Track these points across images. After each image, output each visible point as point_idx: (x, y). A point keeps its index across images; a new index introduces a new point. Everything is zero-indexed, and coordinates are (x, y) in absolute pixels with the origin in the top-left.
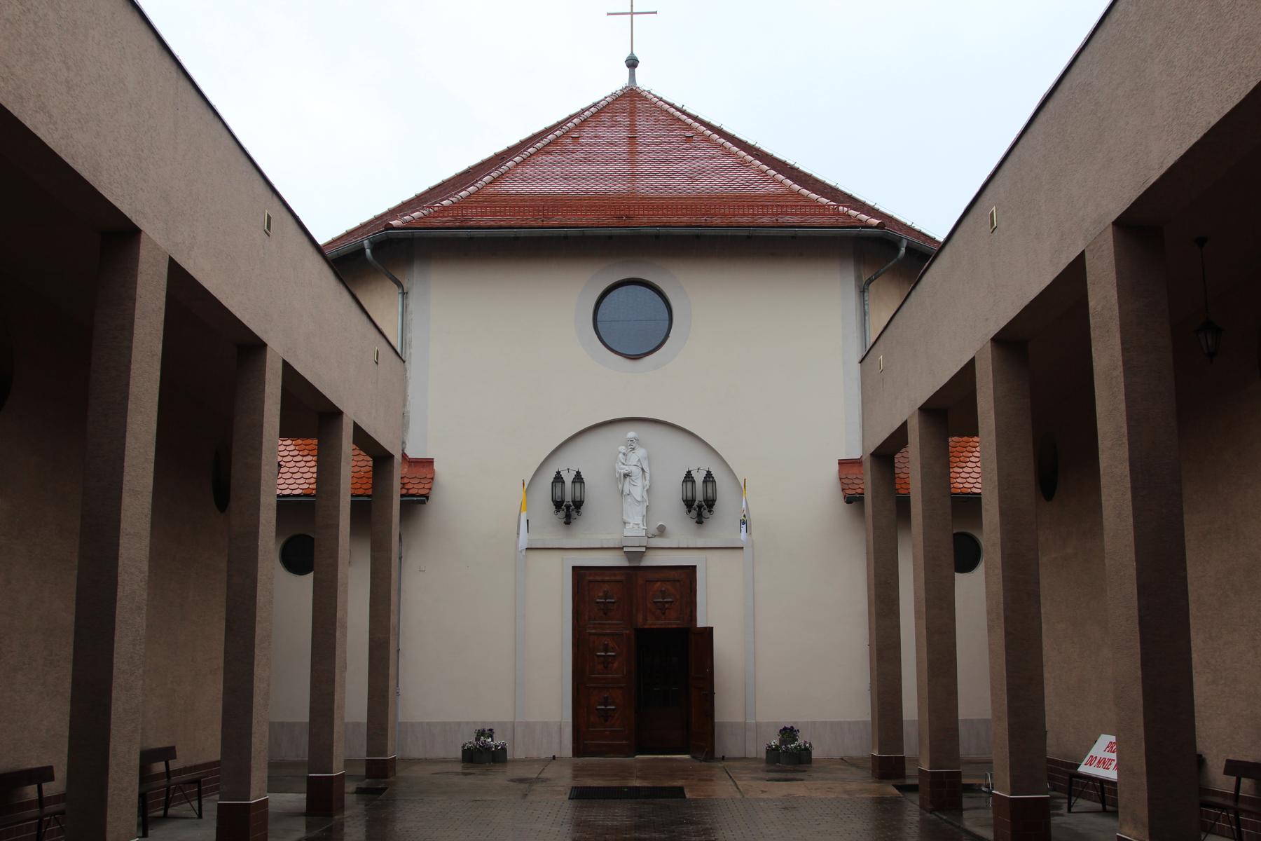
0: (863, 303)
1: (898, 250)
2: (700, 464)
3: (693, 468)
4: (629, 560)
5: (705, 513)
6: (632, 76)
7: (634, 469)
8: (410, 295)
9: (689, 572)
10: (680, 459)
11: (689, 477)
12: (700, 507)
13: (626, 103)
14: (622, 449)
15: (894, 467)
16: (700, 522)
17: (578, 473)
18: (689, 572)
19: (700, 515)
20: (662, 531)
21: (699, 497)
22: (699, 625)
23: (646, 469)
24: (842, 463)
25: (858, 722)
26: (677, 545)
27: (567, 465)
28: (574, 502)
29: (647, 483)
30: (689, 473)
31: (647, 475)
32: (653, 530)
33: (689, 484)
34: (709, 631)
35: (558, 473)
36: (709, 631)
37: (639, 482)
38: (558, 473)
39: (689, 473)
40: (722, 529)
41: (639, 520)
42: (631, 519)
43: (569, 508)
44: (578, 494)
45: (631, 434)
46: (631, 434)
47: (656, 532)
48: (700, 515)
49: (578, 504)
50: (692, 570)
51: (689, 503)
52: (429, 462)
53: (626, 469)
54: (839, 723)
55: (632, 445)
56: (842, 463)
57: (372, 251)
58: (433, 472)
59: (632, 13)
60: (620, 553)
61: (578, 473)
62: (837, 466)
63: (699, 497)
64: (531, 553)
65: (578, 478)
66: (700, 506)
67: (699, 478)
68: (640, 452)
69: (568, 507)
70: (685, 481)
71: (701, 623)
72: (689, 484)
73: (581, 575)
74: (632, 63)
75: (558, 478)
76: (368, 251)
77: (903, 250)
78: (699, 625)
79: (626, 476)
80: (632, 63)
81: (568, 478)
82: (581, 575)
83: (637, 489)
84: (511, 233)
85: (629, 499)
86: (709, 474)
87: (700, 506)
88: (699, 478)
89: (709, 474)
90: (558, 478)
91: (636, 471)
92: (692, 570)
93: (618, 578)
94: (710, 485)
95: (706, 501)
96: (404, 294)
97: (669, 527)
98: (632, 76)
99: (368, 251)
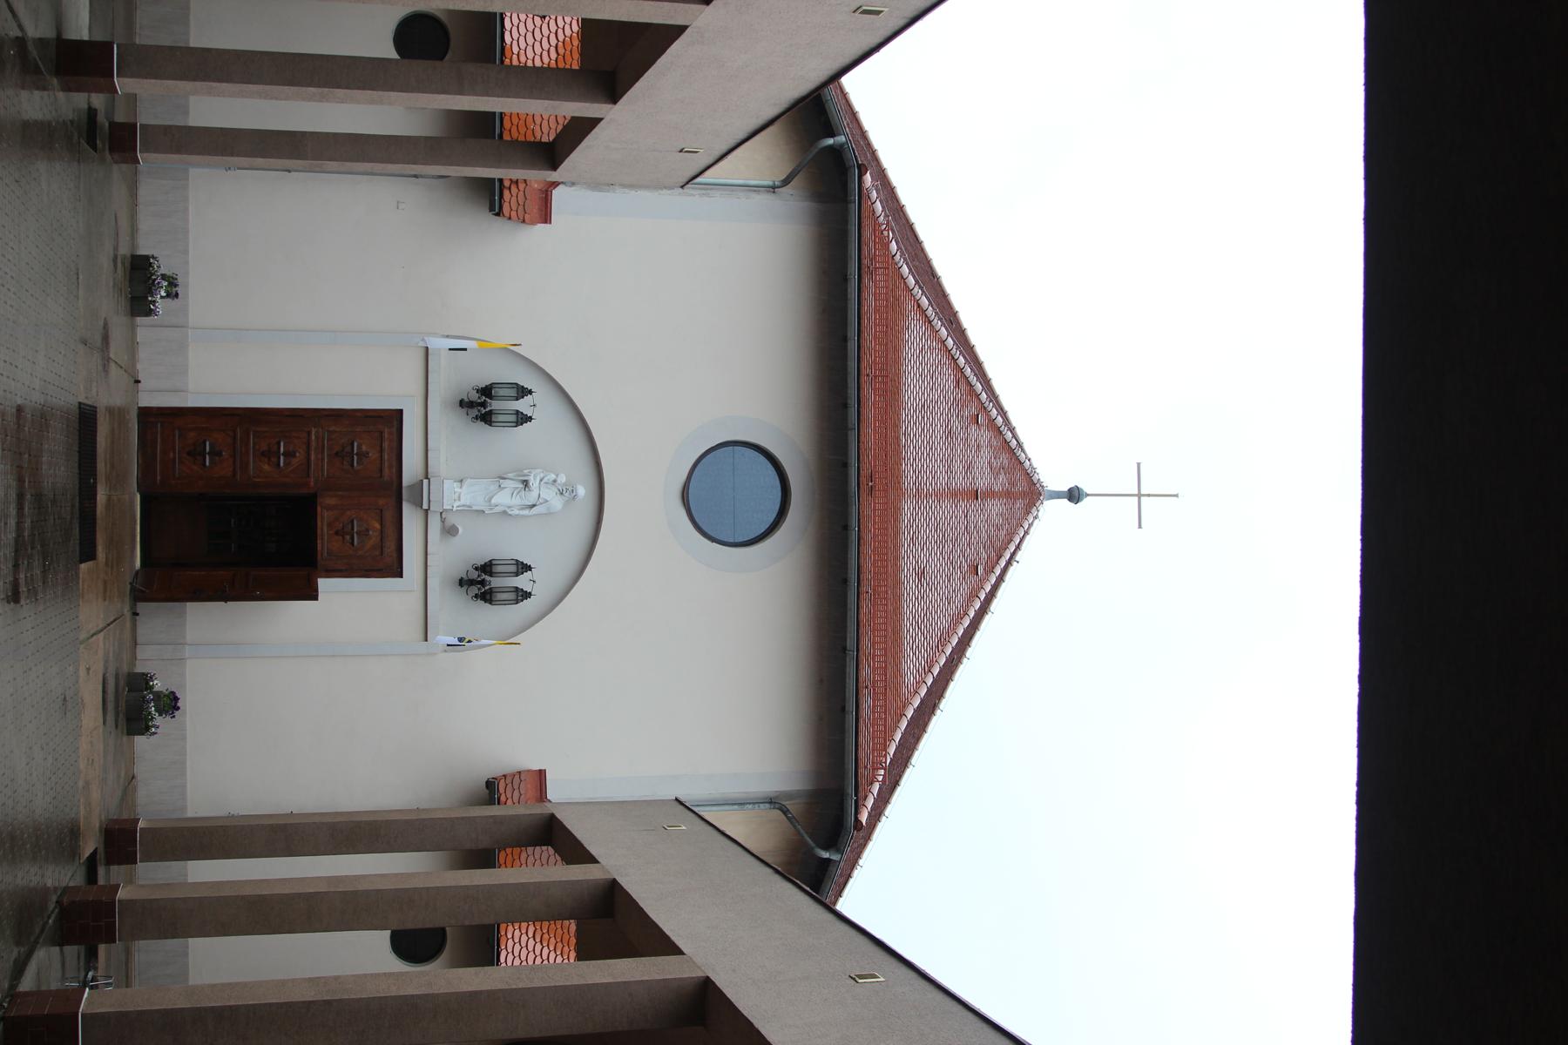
1: (826, 848)
2: (540, 583)
4: (411, 487)
6: (1057, 495)
7: (534, 494)
10: (545, 550)
11: (524, 568)
14: (562, 479)
16: (461, 582)
17: (530, 419)
19: (471, 582)
24: (541, 774)
27: (540, 404)
29: (516, 512)
30: (529, 568)
31: (526, 512)
32: (452, 520)
33: (513, 569)
34: (313, 595)
36: (313, 595)
37: (517, 501)
38: (530, 392)
39: (529, 568)
40: (455, 613)
42: (464, 488)
43: (482, 405)
44: (501, 418)
45: (581, 491)
46: (581, 491)
48: (471, 582)
49: (487, 418)
51: (487, 568)
52: (546, 217)
53: (534, 483)
55: (566, 492)
56: (541, 774)
57: (831, 147)
58: (533, 223)
59: (1139, 495)
64: (422, 353)
65: (522, 419)
66: (482, 583)
67: (522, 582)
68: (557, 503)
69: (483, 405)
71: (323, 584)
72: (513, 569)
73: (394, 419)
74: (1074, 495)
75: (523, 392)
76: (830, 141)
77: (825, 855)
79: (526, 483)
80: (1074, 495)
81: (523, 405)
82: (394, 419)
83: (506, 498)
85: (493, 487)
86: (527, 595)
87: (482, 583)
88: (522, 582)
89: (527, 595)
90: (523, 392)
91: (532, 497)
93: (386, 471)
96: (773, 189)
97: (456, 540)
98: (1057, 495)
99: (830, 141)
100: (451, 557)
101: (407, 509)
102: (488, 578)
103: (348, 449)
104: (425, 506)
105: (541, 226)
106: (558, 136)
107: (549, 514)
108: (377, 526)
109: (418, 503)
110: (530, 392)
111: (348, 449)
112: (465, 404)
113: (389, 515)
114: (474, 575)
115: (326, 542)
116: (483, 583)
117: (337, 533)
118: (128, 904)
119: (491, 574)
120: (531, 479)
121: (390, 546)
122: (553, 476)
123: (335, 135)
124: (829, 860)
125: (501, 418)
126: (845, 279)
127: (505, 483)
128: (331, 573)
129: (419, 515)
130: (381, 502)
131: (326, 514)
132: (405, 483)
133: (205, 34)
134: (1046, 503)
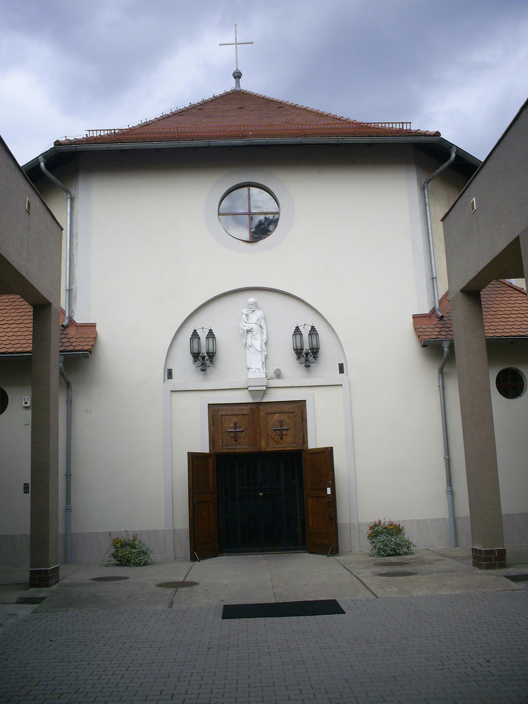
1: (450, 155)
2: (305, 320)
4: (253, 397)
5: (311, 358)
6: (238, 84)
7: (255, 327)
8: (76, 200)
9: (301, 404)
10: (287, 319)
12: (307, 354)
13: (194, 336)
14: (245, 311)
15: (481, 305)
16: (308, 366)
17: (211, 331)
18: (301, 404)
19: (307, 360)
20: (278, 375)
21: (307, 347)
22: (310, 447)
24: (415, 317)
25: (437, 520)
27: (202, 324)
29: (265, 337)
30: (297, 328)
31: (265, 331)
32: (271, 374)
33: (298, 337)
34: (327, 454)
35: (195, 331)
36: (327, 454)
37: (258, 336)
38: (195, 331)
39: (297, 328)
40: (326, 370)
41: (259, 365)
42: (253, 364)
43: (204, 359)
44: (211, 347)
45: (251, 300)
46: (251, 300)
47: (273, 375)
48: (307, 360)
49: (212, 355)
50: (302, 403)
51: (299, 352)
52: (93, 326)
53: (248, 327)
54: (425, 521)
55: (254, 308)
56: (415, 317)
57: (46, 165)
58: (96, 333)
59: (236, 44)
60: (246, 392)
61: (211, 331)
62: (411, 320)
63: (307, 347)
64: (175, 395)
65: (211, 335)
66: (308, 355)
67: (305, 332)
68: (259, 313)
69: (203, 358)
71: (315, 441)
72: (298, 337)
73: (214, 409)
74: (237, 76)
75: (195, 335)
76: (42, 164)
77: (453, 155)
78: (310, 447)
79: (248, 331)
80: (237, 76)
81: (203, 335)
82: (214, 409)
83: (257, 342)
85: (252, 350)
86: (313, 328)
87: (308, 355)
88: (305, 332)
89: (313, 328)
90: (195, 335)
91: (255, 327)
92: (302, 403)
93: (245, 412)
94: (314, 337)
95: (312, 349)
96: (72, 200)
97: (283, 371)
98: (238, 84)
99: (42, 164)
102: (304, 351)
103: (232, 434)
104: (264, 388)
105: (98, 329)
106: (30, 304)
107: (265, 318)
108: (277, 415)
109: (264, 393)
110: (195, 331)
111: (232, 434)
113: (270, 409)
114: (303, 359)
115: (288, 444)
117: (282, 439)
119: (302, 349)
120: (245, 328)
121: (287, 408)
122: (244, 316)
123: (32, 443)
124: (457, 155)
125: (211, 347)
126: (122, 151)
130: (262, 414)
132: (251, 401)
133: (20, 522)
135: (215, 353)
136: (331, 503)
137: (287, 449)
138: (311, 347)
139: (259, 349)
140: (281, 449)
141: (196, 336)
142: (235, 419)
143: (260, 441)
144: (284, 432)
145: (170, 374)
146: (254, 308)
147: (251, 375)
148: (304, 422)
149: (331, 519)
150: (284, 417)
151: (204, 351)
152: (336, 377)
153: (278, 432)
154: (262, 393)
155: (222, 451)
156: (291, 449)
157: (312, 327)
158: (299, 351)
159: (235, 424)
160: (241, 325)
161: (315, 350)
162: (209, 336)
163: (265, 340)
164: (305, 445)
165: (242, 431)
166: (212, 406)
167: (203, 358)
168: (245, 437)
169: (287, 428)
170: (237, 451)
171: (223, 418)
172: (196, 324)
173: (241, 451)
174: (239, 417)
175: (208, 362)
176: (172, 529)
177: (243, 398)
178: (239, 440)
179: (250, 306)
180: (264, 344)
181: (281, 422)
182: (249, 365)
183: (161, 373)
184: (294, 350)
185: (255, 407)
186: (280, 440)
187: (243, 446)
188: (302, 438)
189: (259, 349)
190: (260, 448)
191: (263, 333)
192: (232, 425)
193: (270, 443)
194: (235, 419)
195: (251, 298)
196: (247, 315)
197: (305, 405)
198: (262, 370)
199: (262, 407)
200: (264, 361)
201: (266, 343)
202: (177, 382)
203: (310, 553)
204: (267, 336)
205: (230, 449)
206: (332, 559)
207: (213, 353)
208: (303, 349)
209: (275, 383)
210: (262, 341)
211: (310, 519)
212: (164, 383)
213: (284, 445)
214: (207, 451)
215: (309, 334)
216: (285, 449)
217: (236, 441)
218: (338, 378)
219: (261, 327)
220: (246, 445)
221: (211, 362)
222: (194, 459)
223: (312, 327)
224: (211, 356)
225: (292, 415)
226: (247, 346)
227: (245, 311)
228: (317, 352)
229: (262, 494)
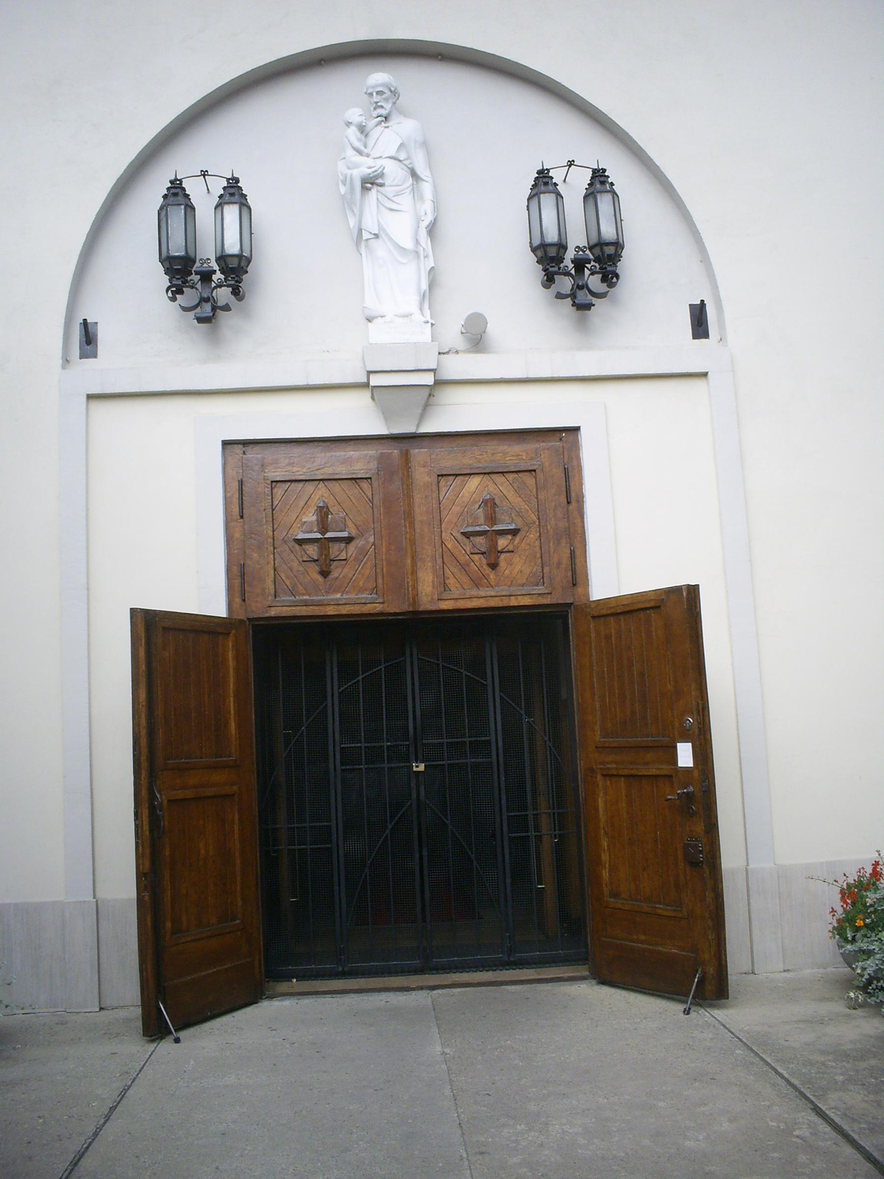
0: (87, 405)
2: (571, 150)
3: (554, 162)
4: (387, 415)
11: (543, 181)
13: (171, 199)
20: (477, 339)
23: (422, 171)
26: (520, 369)
28: (222, 259)
31: (427, 188)
32: (453, 335)
34: (673, 617)
36: (673, 617)
37: (405, 201)
40: (644, 320)
41: (410, 302)
43: (209, 284)
47: (459, 342)
49: (236, 269)
50: (566, 436)
51: (549, 257)
53: (365, 167)
60: (363, 398)
64: (101, 409)
65: (233, 192)
66: (581, 272)
69: (206, 276)
70: (535, 194)
71: (617, 570)
75: (176, 192)
79: (370, 182)
84: (361, 983)
85: (380, 248)
86: (599, 177)
87: (581, 272)
89: (599, 177)
90: (176, 192)
91: (394, 172)
92: (566, 436)
100: (527, 325)
101: (463, 413)
102: (570, 254)
103: (312, 551)
104: (429, 379)
112: (208, 315)
115: (516, 585)
116: (580, 265)
117: (494, 566)
118: (239, 577)
119: (562, 247)
120: (357, 174)
122: (352, 133)
127: (370, 224)
128: (577, 574)
129: (451, 396)
130: (421, 476)
131: (456, 592)
132: (379, 428)
134: (168, 277)
135: (249, 260)
136: (697, 798)
137: (514, 602)
138: (594, 240)
139: (409, 244)
140: (493, 603)
141: (180, 199)
142: (320, 495)
143: (414, 572)
144: (502, 542)
145: (89, 338)
146: (388, 106)
147: (378, 334)
148: (574, 504)
149: (695, 864)
150: (502, 488)
151: (207, 252)
152: (683, 351)
153: (480, 540)
154: (426, 392)
155: (273, 612)
156: (526, 601)
157: (595, 171)
158: (552, 252)
159: (323, 512)
160: (341, 167)
161: (610, 250)
162: (227, 198)
163: (429, 218)
164: (580, 590)
165: (349, 540)
166: (238, 449)
167: (206, 276)
168: (358, 561)
169: (512, 527)
170: (331, 611)
171: (279, 491)
172: (181, 163)
173: (345, 610)
174: (336, 487)
175: (223, 295)
176: (91, 898)
177: (356, 417)
178: (336, 572)
179: (376, 98)
180: (423, 234)
181: (490, 505)
182: (372, 304)
183: (50, 332)
184: (534, 250)
185: (395, 452)
186: (487, 570)
187: (351, 595)
188: (566, 561)
189: (409, 244)
190: (416, 596)
191: (422, 198)
192: (311, 517)
193: (451, 581)
194: (320, 495)
195: (379, 76)
196: (362, 129)
197: (575, 447)
198: (418, 317)
199: (419, 454)
200: (425, 286)
201: (432, 230)
202: (109, 368)
203: (603, 982)
204: (436, 207)
205: (306, 604)
206: (703, 1016)
207: (240, 256)
208: (565, 248)
209: (463, 365)
210: (419, 220)
211: (605, 857)
212: (64, 367)
213: (503, 590)
214: (215, 604)
215: (586, 197)
216: (505, 602)
217: (325, 574)
218: (692, 354)
219: (414, 174)
220: (361, 590)
221: (236, 292)
222: (159, 637)
223: (595, 171)
224: (233, 270)
225: (529, 480)
226: (366, 235)
227: (355, 115)
228: (615, 258)
229: (422, 767)
